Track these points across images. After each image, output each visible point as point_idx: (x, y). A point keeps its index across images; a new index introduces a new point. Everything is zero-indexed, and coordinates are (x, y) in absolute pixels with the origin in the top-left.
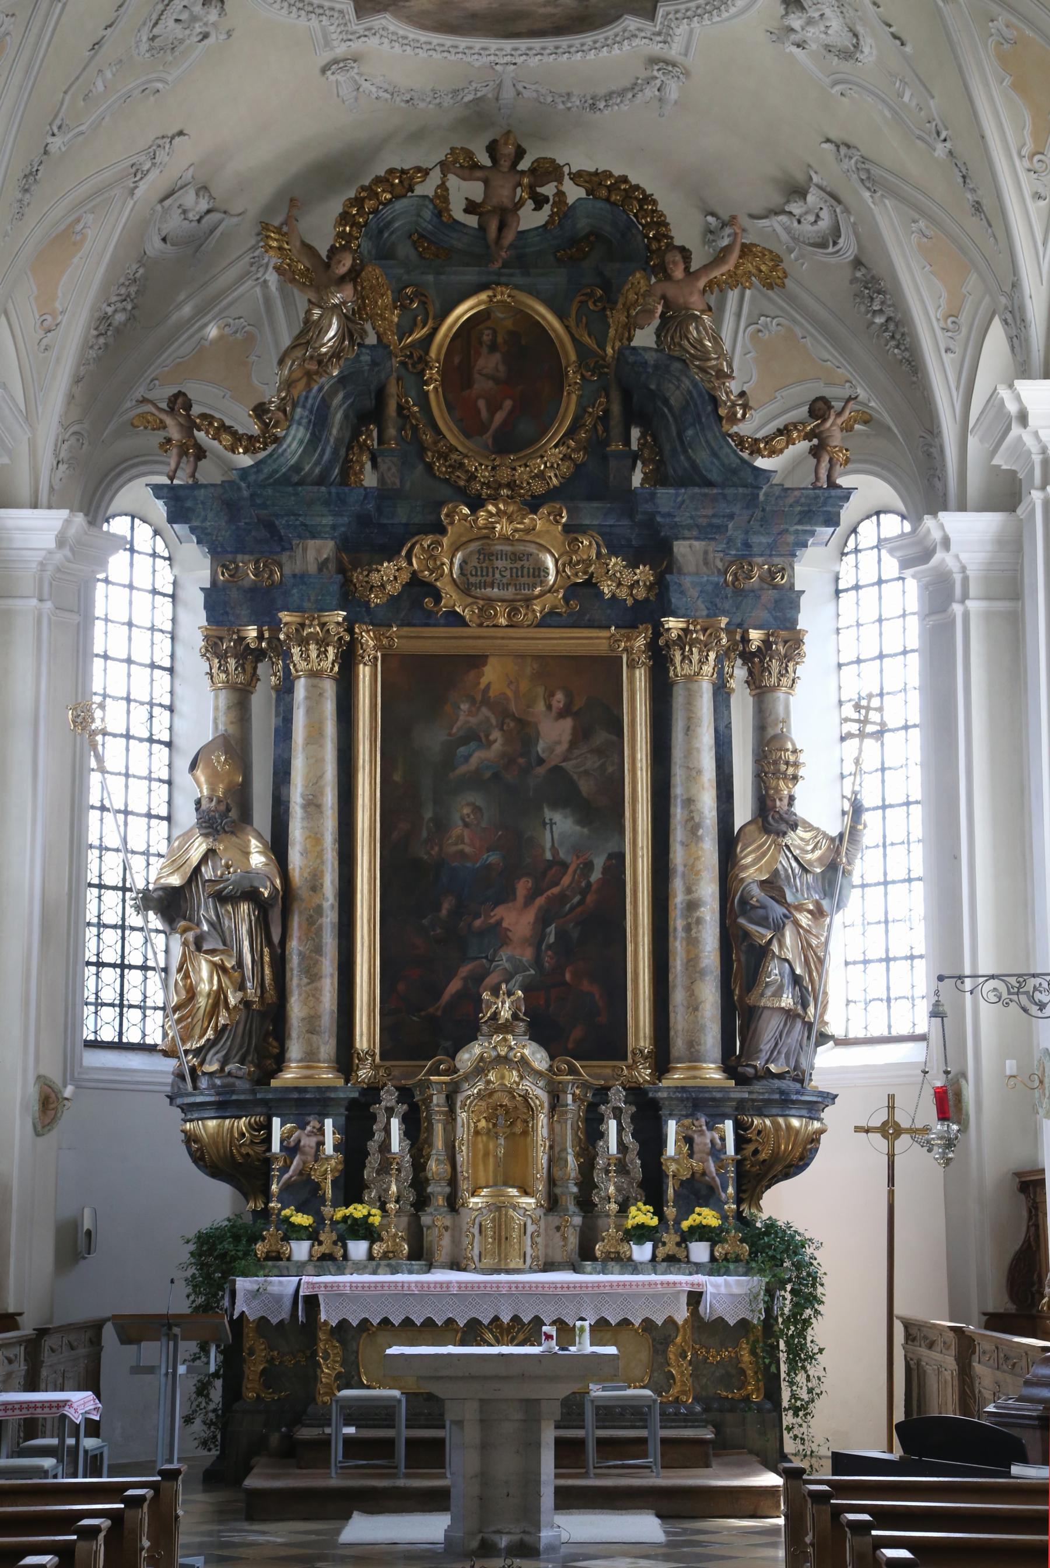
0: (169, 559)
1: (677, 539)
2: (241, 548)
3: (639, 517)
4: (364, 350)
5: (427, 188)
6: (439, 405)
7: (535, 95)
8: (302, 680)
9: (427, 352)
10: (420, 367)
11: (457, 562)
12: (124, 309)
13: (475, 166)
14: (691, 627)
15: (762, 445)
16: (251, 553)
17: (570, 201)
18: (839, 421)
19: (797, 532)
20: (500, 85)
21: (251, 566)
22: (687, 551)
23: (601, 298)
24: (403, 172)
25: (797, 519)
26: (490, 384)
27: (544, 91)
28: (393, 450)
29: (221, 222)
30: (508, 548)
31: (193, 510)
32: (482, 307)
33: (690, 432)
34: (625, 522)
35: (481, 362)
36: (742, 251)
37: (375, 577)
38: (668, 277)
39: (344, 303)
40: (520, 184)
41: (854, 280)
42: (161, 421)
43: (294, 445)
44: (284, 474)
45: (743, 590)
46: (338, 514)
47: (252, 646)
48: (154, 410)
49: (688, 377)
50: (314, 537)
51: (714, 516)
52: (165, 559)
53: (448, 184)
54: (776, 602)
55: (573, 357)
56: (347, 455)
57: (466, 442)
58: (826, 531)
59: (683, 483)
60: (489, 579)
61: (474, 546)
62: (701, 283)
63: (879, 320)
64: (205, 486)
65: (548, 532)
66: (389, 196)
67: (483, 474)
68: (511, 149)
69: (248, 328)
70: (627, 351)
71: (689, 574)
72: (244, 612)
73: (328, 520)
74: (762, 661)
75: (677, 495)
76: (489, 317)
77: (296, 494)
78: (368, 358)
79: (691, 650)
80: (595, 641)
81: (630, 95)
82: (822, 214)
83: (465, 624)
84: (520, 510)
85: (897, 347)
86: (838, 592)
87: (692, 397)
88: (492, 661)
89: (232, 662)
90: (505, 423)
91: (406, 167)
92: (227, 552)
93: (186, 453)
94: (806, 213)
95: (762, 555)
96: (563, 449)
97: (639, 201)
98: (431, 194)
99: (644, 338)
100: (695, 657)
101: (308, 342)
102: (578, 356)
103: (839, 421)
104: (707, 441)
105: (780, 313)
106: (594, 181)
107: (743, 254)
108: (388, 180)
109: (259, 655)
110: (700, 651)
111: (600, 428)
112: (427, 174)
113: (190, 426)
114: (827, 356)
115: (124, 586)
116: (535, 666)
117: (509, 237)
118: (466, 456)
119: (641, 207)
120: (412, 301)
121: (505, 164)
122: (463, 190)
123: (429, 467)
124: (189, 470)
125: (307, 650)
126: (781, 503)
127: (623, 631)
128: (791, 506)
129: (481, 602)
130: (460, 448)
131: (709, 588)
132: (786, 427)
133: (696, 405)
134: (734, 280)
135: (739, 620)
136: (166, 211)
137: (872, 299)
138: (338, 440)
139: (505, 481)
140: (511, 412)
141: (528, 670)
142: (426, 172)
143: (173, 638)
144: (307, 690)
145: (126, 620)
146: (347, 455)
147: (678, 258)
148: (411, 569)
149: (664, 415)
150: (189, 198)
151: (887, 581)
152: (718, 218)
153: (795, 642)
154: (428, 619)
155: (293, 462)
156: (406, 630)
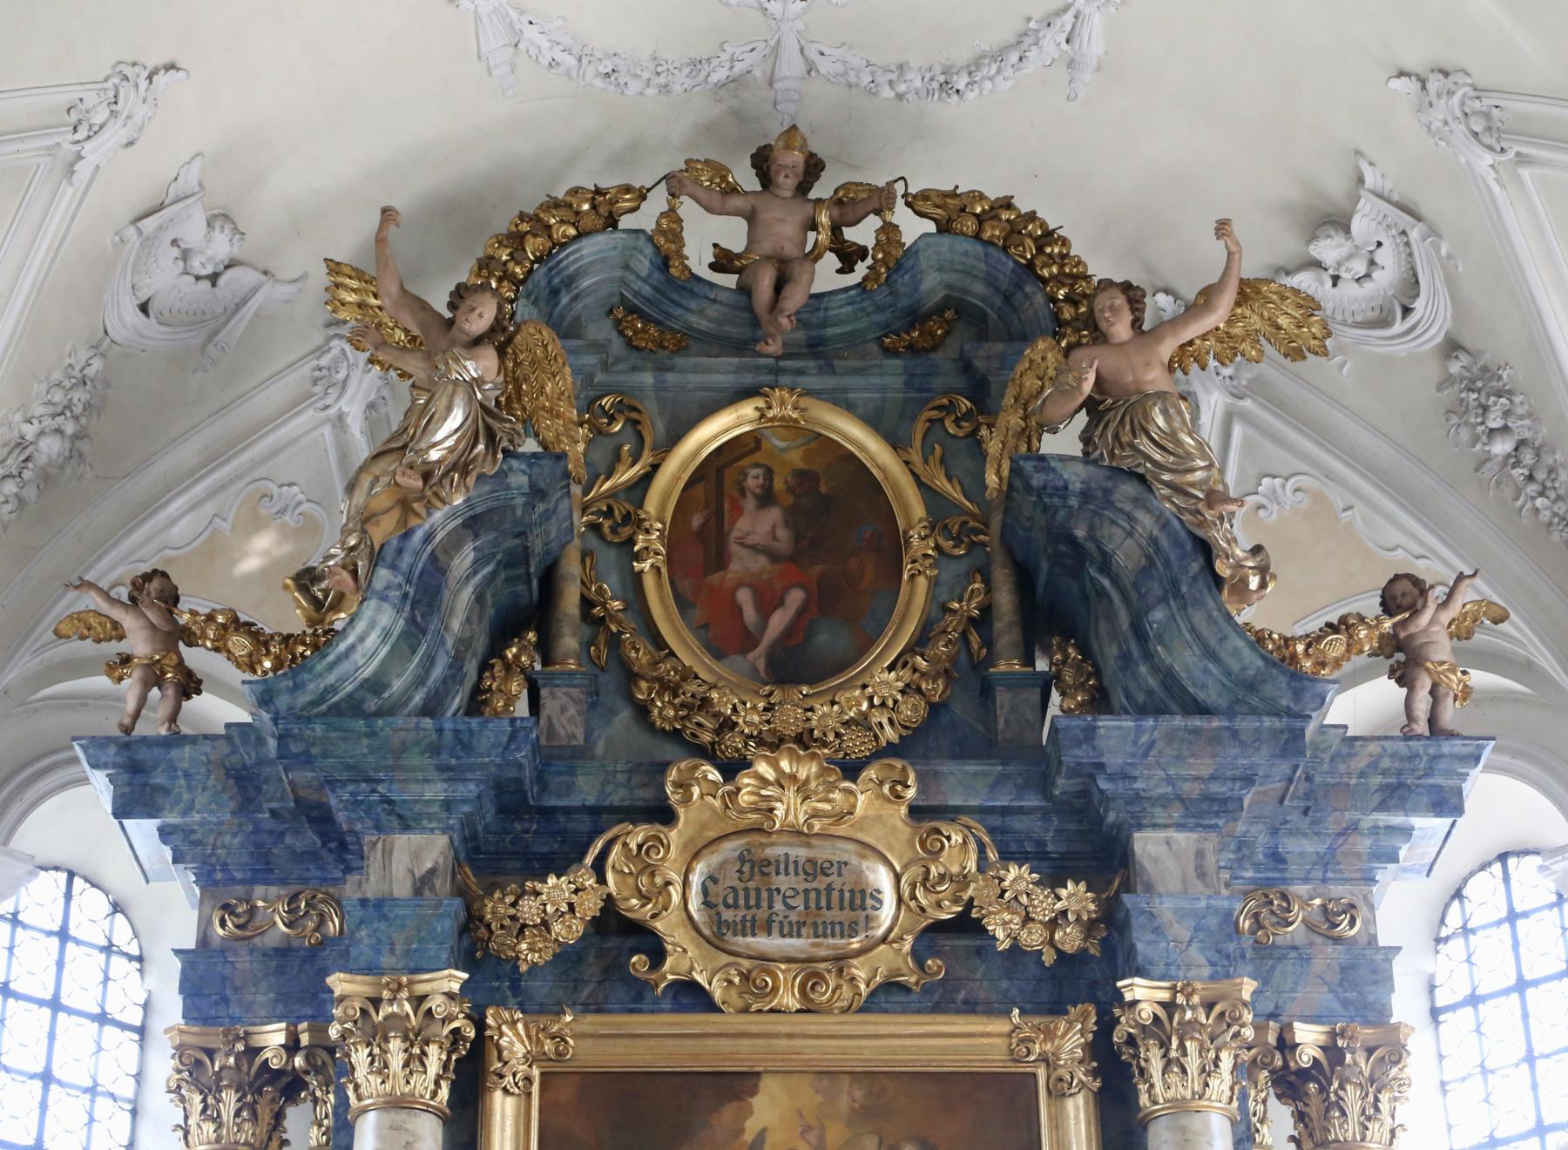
0: (140, 959)
1: (1140, 827)
2: (263, 870)
3: (1063, 785)
4: (515, 463)
5: (646, 218)
6: (662, 598)
7: (839, 68)
8: (371, 1118)
9: (640, 505)
10: (626, 531)
11: (696, 879)
12: (59, 431)
13: (733, 190)
14: (1180, 999)
15: (1300, 648)
16: (283, 882)
17: (908, 239)
18: (1445, 617)
19: (1375, 830)
20: (776, 50)
21: (282, 907)
22: (1159, 849)
23: (968, 415)
24: (598, 191)
25: (1376, 798)
26: (762, 561)
27: (856, 62)
28: (571, 674)
29: (255, 290)
30: (802, 853)
31: (166, 791)
32: (746, 428)
33: (1158, 615)
34: (1032, 801)
35: (742, 525)
36: (1241, 293)
37: (529, 909)
38: (1100, 337)
39: (479, 382)
40: (814, 226)
41: (1447, 381)
42: (116, 625)
43: (372, 640)
44: (350, 696)
45: (1274, 946)
46: (452, 774)
47: (275, 1064)
48: (104, 607)
49: (1148, 510)
50: (406, 828)
51: (1213, 778)
52: (130, 958)
53: (681, 212)
54: (1343, 970)
55: (918, 510)
56: (480, 678)
57: (716, 666)
58: (1428, 826)
59: (1150, 708)
60: (762, 914)
61: (731, 848)
62: (1167, 349)
63: (1501, 447)
64: (193, 740)
65: (879, 819)
66: (572, 232)
67: (750, 718)
68: (797, 158)
69: (305, 507)
70: (1027, 465)
71: (1170, 894)
72: (262, 998)
73: (436, 791)
74: (1323, 1089)
75: (1139, 731)
76: (758, 442)
77: (373, 734)
78: (524, 480)
79: (1182, 1046)
80: (976, 1040)
81: (1014, 57)
82: (1383, 256)
83: (712, 1007)
84: (823, 772)
85: (1542, 494)
86: (1435, 1013)
87: (1158, 550)
88: (767, 1083)
89: (230, 1099)
90: (788, 633)
91: (603, 185)
92: (234, 881)
93: (159, 681)
94: (1350, 257)
95: (1306, 880)
96: (906, 674)
97: (1036, 239)
98: (650, 226)
99: (1063, 442)
100: (1193, 1063)
101: (405, 446)
102: (929, 509)
103: (1445, 617)
104: (1193, 630)
105: (1306, 468)
106: (948, 210)
107: (1243, 298)
108: (570, 206)
109: (291, 1087)
110: (1202, 1050)
111: (975, 639)
112: (643, 197)
113: (176, 635)
114: (1397, 537)
115: (41, 1003)
116: (858, 1094)
117: (794, 299)
118: (713, 687)
119: (1040, 249)
120: (612, 419)
121: (786, 184)
122: (706, 234)
123: (642, 711)
124: (164, 711)
125: (384, 1052)
126: (1342, 767)
127: (1037, 1020)
128: (1362, 774)
129: (746, 964)
130: (702, 675)
131: (1213, 922)
132: (1343, 620)
133: (1167, 563)
134: (1228, 346)
135: (1270, 1007)
136: (148, 242)
137: (1486, 409)
138: (464, 644)
139: (791, 731)
140: (802, 612)
141: (844, 1104)
142: (642, 195)
143: (134, 1113)
144: (380, 1136)
145: (39, 1069)
146: (480, 678)
147: (1120, 300)
148: (603, 891)
149: (1102, 593)
150: (193, 229)
151: (1535, 983)
152: (1177, 297)
153: (1390, 1051)
154: (638, 996)
155: (368, 672)
156: (591, 1022)
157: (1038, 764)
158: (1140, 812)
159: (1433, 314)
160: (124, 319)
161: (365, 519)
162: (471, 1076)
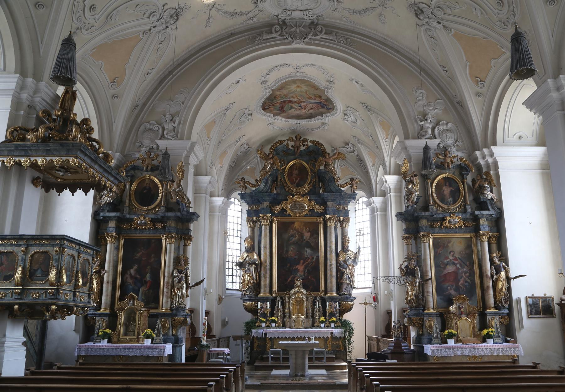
5: (285, 143)
13: (293, 140)
22: (329, 204)
59: (329, 192)
67: (295, 191)
70: (319, 170)
99: (322, 168)
106: (313, 142)
109: (256, 222)
113: (244, 183)
117: (299, 151)
122: (291, 144)
134: (337, 158)
154: (285, 215)
158: (328, 200)
159: (356, 153)
162: (271, 223)
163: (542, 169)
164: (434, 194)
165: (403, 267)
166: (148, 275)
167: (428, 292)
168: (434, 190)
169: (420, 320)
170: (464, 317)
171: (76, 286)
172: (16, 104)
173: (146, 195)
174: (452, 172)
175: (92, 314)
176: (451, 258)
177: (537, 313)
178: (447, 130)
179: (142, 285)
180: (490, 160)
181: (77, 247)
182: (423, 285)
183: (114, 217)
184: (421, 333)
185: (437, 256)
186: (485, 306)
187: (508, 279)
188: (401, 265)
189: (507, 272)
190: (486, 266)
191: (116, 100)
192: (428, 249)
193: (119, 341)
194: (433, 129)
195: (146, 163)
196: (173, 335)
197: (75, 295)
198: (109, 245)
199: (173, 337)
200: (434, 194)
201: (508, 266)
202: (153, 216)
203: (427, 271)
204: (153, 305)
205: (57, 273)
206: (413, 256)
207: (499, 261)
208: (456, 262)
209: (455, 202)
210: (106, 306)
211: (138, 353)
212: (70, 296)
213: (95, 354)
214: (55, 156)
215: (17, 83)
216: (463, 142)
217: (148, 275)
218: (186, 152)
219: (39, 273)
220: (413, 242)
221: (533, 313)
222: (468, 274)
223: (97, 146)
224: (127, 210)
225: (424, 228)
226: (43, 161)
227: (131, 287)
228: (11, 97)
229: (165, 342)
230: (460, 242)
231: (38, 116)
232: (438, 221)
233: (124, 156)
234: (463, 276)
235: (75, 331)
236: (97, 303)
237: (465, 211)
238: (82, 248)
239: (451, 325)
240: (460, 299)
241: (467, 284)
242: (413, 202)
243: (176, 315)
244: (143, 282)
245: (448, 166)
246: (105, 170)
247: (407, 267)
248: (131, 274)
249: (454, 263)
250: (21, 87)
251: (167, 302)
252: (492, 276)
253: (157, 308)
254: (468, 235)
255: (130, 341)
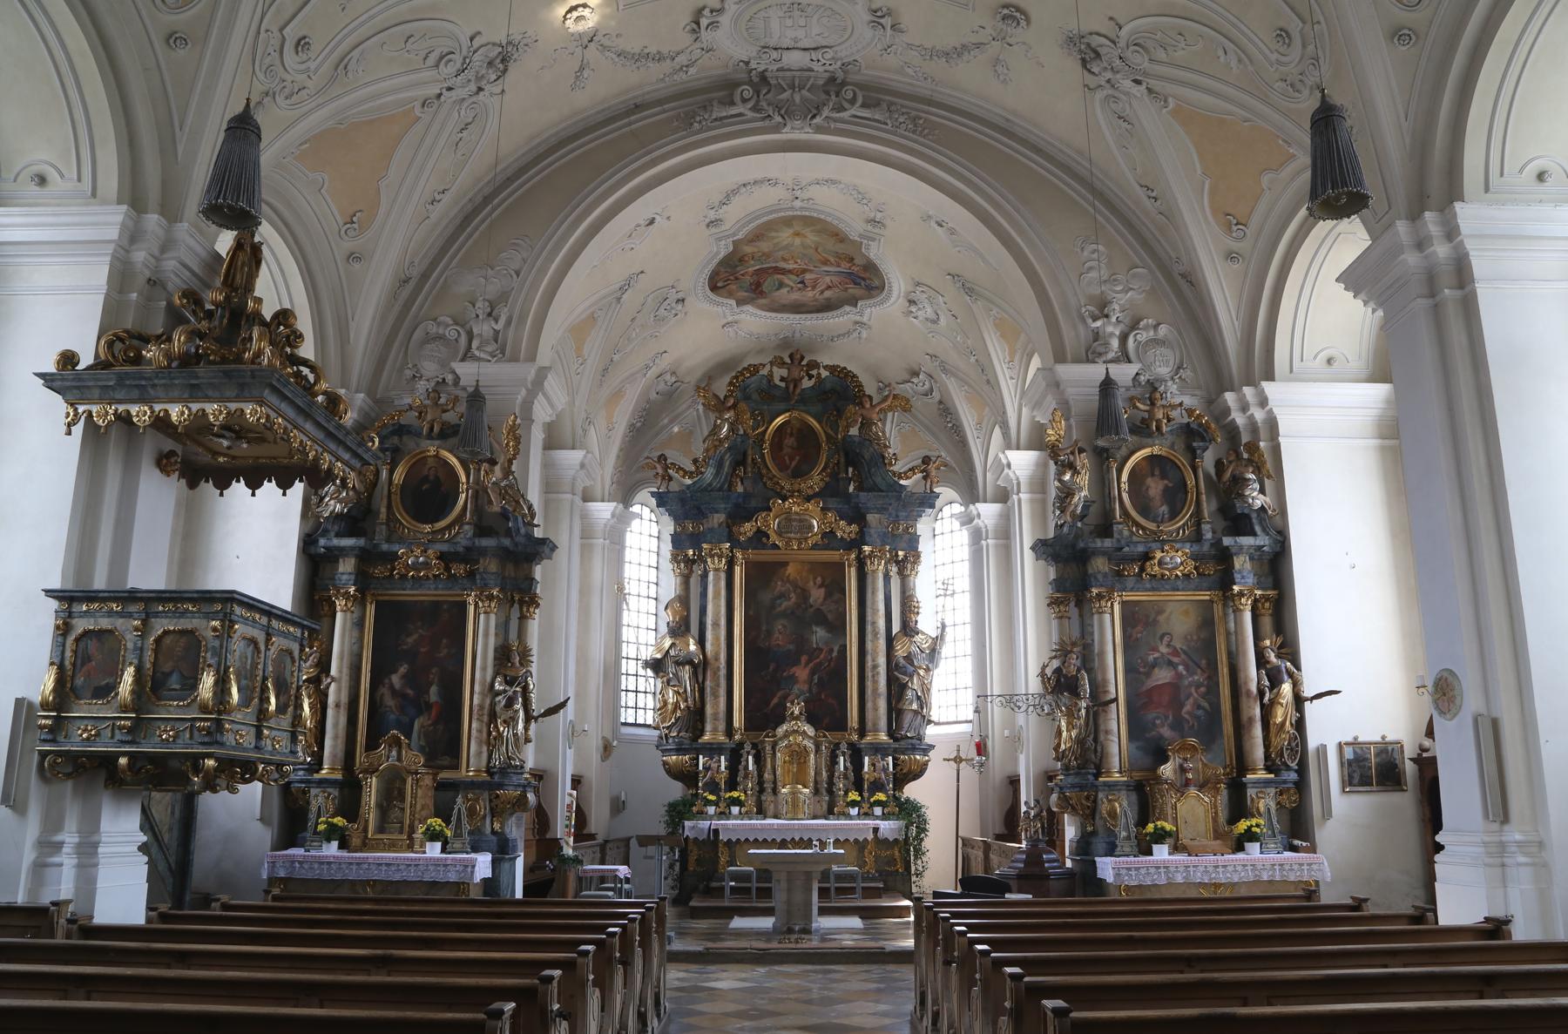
5: (764, 372)
22: (872, 518)
59: (870, 490)
67: (788, 487)
99: (854, 431)
106: (832, 369)
109: (694, 562)
113: (666, 468)
122: (779, 372)
134: (891, 408)
154: (764, 547)
157: (847, 497)
160: (653, 396)
161: (707, 450)
162: (731, 564)
163: (1382, 437)
164: (1125, 496)
165: (1049, 672)
166: (434, 689)
167: (1107, 732)
168: (1125, 486)
169: (1087, 798)
170: (1193, 791)
171: (262, 714)
172: (121, 276)
173: (429, 496)
174: (1168, 443)
175: (301, 782)
176: (1164, 649)
177: (1365, 781)
178: (1156, 342)
179: (420, 713)
180: (1259, 415)
181: (264, 620)
182: (1096, 715)
183: (352, 548)
184: (1089, 829)
185: (1130, 645)
186: (1242, 764)
187: (1299, 701)
188: (1044, 667)
189: (1296, 685)
190: (1246, 669)
191: (357, 266)
192: (1110, 628)
193: (365, 845)
194: (1123, 339)
195: (429, 417)
196: (493, 832)
197: (259, 735)
198: (339, 616)
199: (494, 838)
200: (1125, 496)
201: (1299, 669)
202: (444, 548)
203: (1105, 681)
204: (446, 761)
205: (216, 683)
206: (1074, 644)
207: (1278, 656)
208: (1176, 660)
209: (1174, 515)
210: (333, 762)
211: (412, 876)
212: (248, 738)
213: (310, 876)
214: (210, 400)
215: (123, 225)
216: (1194, 371)
217: (434, 689)
218: (524, 392)
219: (174, 682)
220: (1073, 611)
221: (1356, 781)
222: (1203, 689)
223: (311, 378)
224: (381, 531)
225: (1100, 577)
226: (183, 413)
227: (392, 717)
228: (108, 259)
229: (476, 849)
230: (1186, 613)
231: (170, 305)
232: (1133, 560)
233: (376, 401)
234: (1190, 695)
235: (261, 819)
236: (312, 755)
237: (1197, 537)
238: (275, 623)
239: (1162, 810)
240: (1184, 748)
241: (1200, 712)
242: (1073, 514)
243: (500, 786)
244: (422, 707)
245: (1159, 428)
246: (329, 434)
247: (1058, 671)
248: (392, 687)
249: (1170, 663)
250: (132, 236)
251: (479, 753)
252: (1261, 694)
253: (456, 767)
254: (1205, 596)
255: (392, 846)
